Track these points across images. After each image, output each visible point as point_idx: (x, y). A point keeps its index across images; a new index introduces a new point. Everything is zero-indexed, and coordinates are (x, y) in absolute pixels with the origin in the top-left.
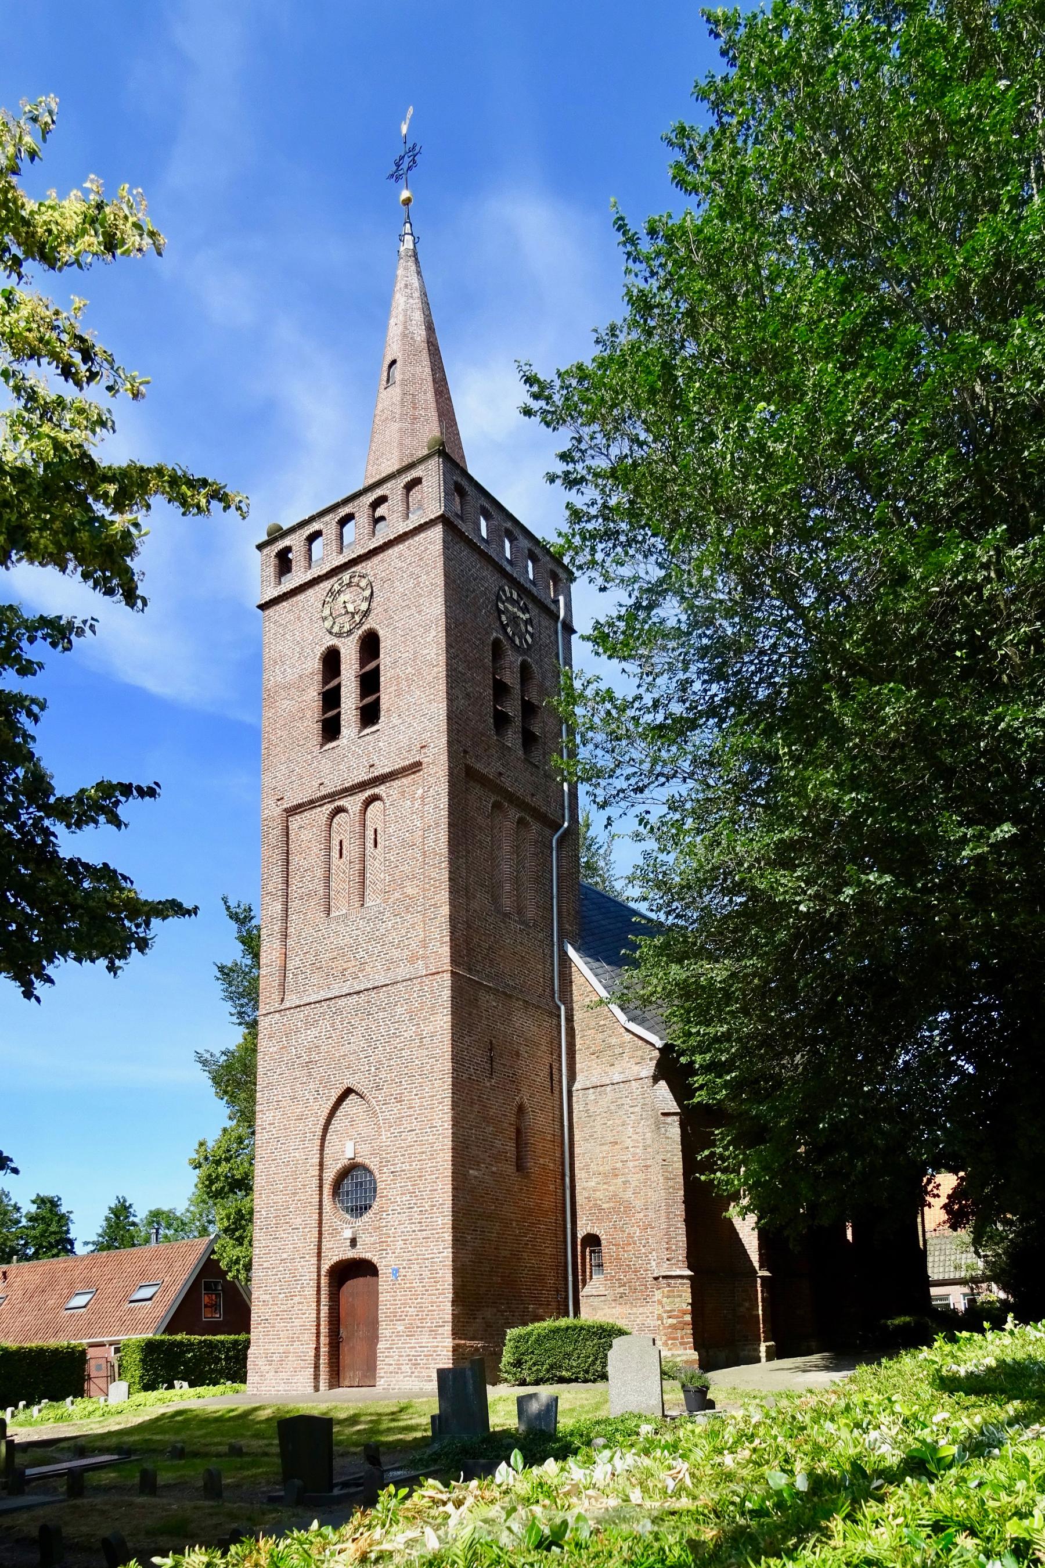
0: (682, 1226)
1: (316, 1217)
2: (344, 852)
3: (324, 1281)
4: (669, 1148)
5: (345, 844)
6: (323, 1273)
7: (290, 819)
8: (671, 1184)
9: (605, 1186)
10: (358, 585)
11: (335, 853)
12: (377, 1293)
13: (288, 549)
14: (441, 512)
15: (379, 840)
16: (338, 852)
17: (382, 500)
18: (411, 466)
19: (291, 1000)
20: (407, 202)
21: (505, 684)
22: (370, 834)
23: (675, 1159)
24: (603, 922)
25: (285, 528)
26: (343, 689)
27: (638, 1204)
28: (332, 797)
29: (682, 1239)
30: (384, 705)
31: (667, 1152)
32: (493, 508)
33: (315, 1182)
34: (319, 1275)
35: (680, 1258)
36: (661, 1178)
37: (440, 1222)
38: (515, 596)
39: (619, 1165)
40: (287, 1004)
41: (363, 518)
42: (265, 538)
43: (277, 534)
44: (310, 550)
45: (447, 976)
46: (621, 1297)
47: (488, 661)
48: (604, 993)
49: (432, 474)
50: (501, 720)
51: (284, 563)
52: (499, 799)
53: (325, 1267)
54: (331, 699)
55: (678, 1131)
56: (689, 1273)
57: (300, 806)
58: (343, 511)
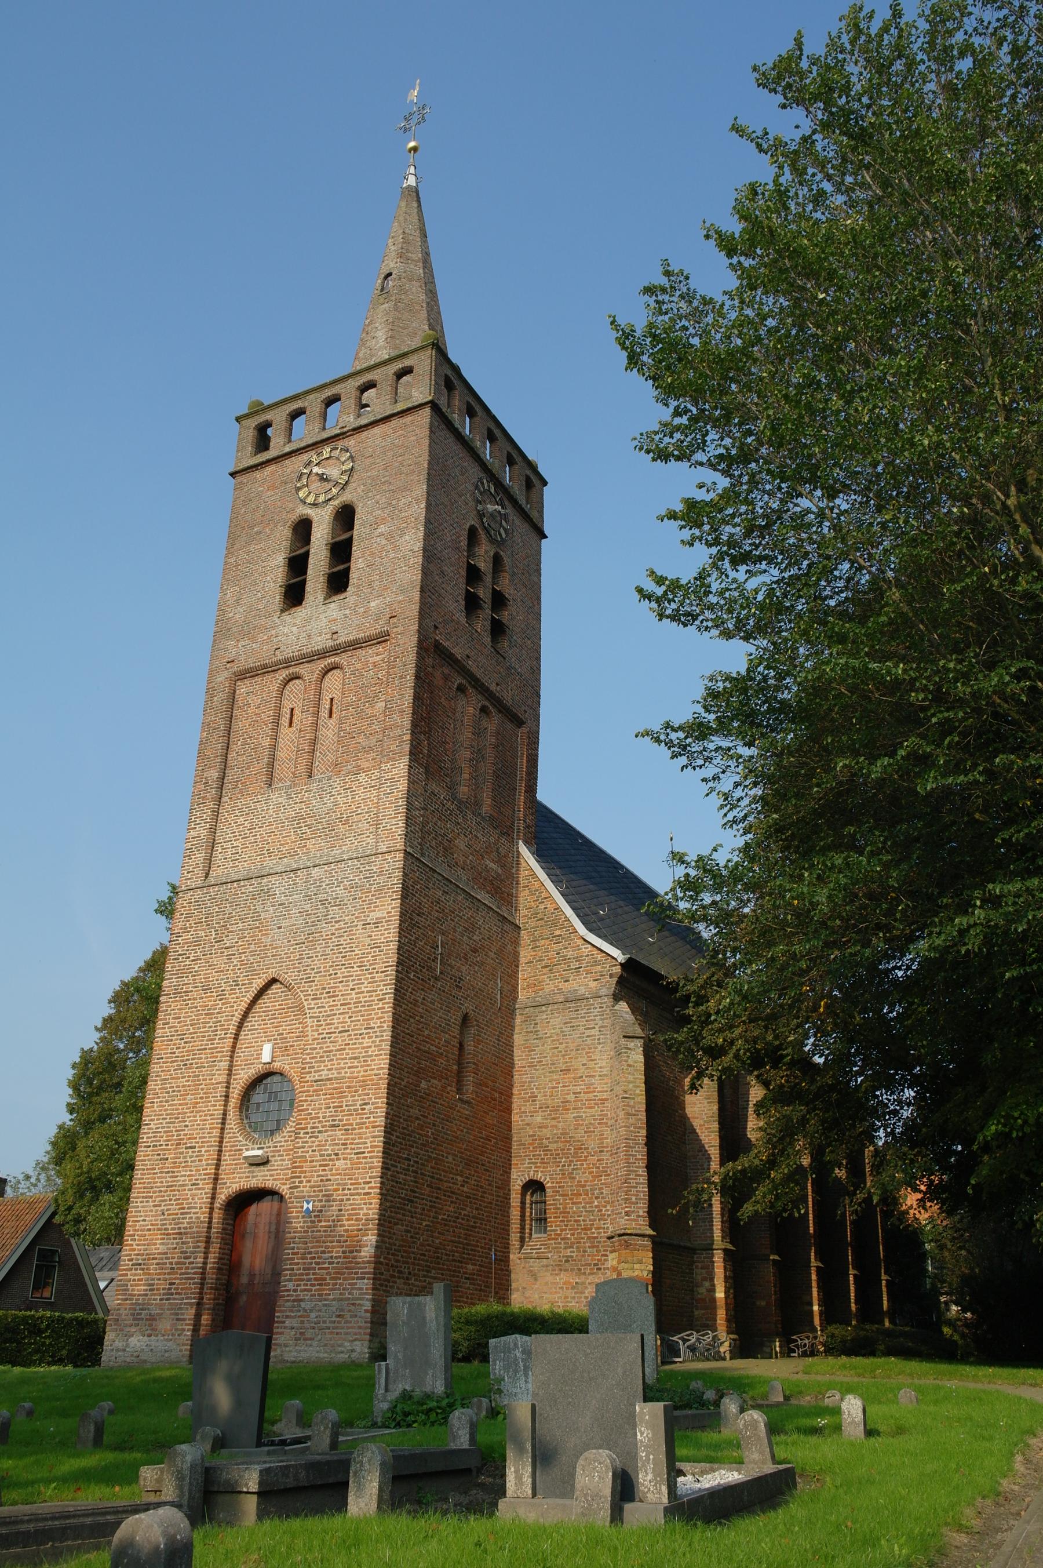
0: (642, 1172)
1: (216, 1132)
2: (295, 720)
3: (217, 1215)
4: (631, 1078)
5: (296, 712)
6: (217, 1205)
7: (239, 683)
8: (632, 1120)
9: (554, 1123)
10: (338, 459)
11: (285, 720)
12: (647, 1137)
13: (268, 424)
14: (430, 398)
15: (334, 710)
16: (287, 721)
17: (371, 385)
18: (404, 355)
19: (212, 880)
20: (415, 149)
21: (479, 570)
22: (326, 704)
23: (638, 1092)
24: (555, 835)
25: (266, 404)
26: (311, 556)
27: (593, 1144)
28: (287, 663)
29: (642, 1188)
30: (354, 575)
31: (630, 1082)
32: (475, 407)
33: (221, 1089)
34: (212, 1209)
35: (641, 1213)
36: (622, 1114)
37: (369, 1145)
38: (492, 491)
39: (571, 1097)
40: (212, 880)
41: (349, 401)
42: (246, 411)
43: (258, 408)
44: (291, 425)
45: (400, 856)
46: (567, 1261)
47: (464, 543)
48: (73, 1241)
49: (424, 363)
50: (472, 603)
51: (262, 441)
52: (464, 682)
53: (222, 1197)
54: (298, 565)
55: (641, 1058)
56: (652, 1233)
57: (248, 671)
58: (328, 393)
